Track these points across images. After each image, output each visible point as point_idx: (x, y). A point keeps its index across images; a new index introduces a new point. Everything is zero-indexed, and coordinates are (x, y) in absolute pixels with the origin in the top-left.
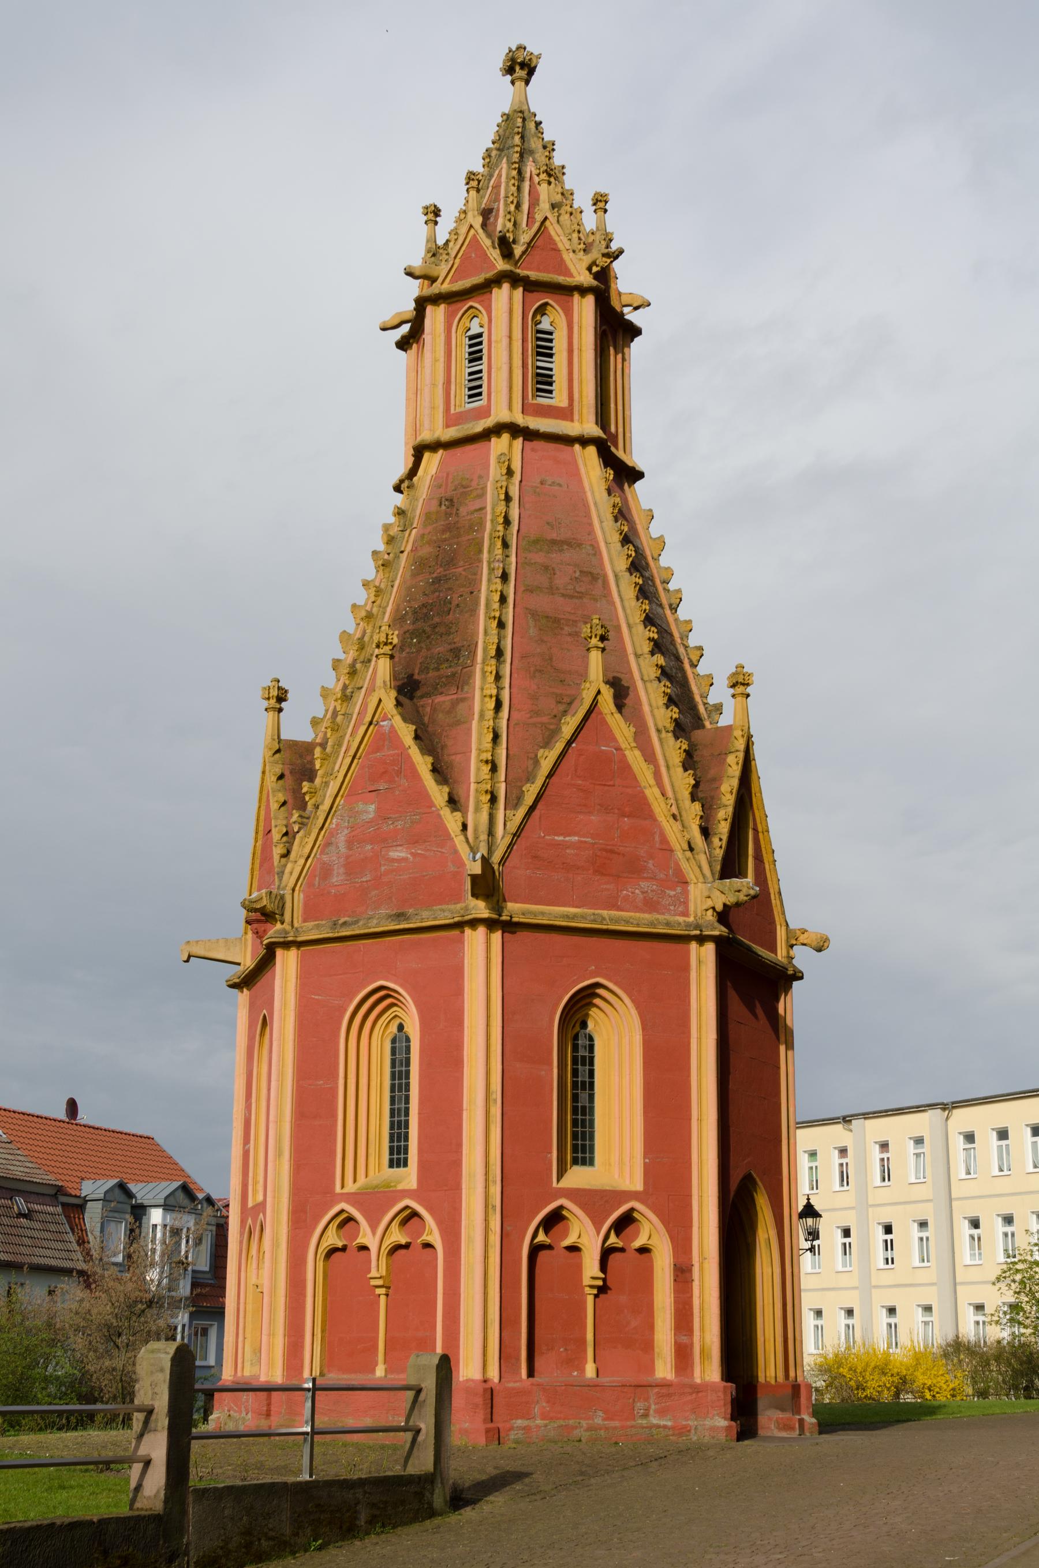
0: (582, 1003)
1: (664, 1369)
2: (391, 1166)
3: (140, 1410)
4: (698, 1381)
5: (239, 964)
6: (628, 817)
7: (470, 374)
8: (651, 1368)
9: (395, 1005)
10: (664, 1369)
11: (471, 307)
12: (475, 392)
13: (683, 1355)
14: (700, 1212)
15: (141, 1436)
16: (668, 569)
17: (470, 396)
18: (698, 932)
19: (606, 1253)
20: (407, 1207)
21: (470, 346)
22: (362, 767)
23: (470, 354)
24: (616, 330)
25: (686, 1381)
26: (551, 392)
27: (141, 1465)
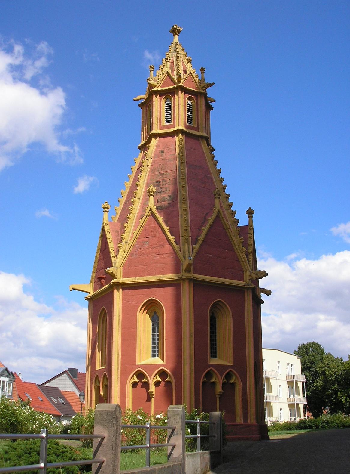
0: (216, 306)
1: (239, 420)
2: (153, 356)
3: (170, 428)
4: (249, 423)
5: (89, 293)
6: (227, 250)
7: (167, 115)
8: (234, 420)
9: (154, 306)
10: (239, 420)
11: (167, 95)
12: (168, 120)
13: (245, 415)
14: (249, 372)
15: (170, 437)
16: (222, 178)
17: (166, 121)
18: (248, 286)
19: (224, 384)
20: (139, 370)
21: (166, 107)
22: (143, 230)
23: (166, 109)
24: (209, 108)
25: (246, 424)
26: (191, 122)
27: (172, 447)
